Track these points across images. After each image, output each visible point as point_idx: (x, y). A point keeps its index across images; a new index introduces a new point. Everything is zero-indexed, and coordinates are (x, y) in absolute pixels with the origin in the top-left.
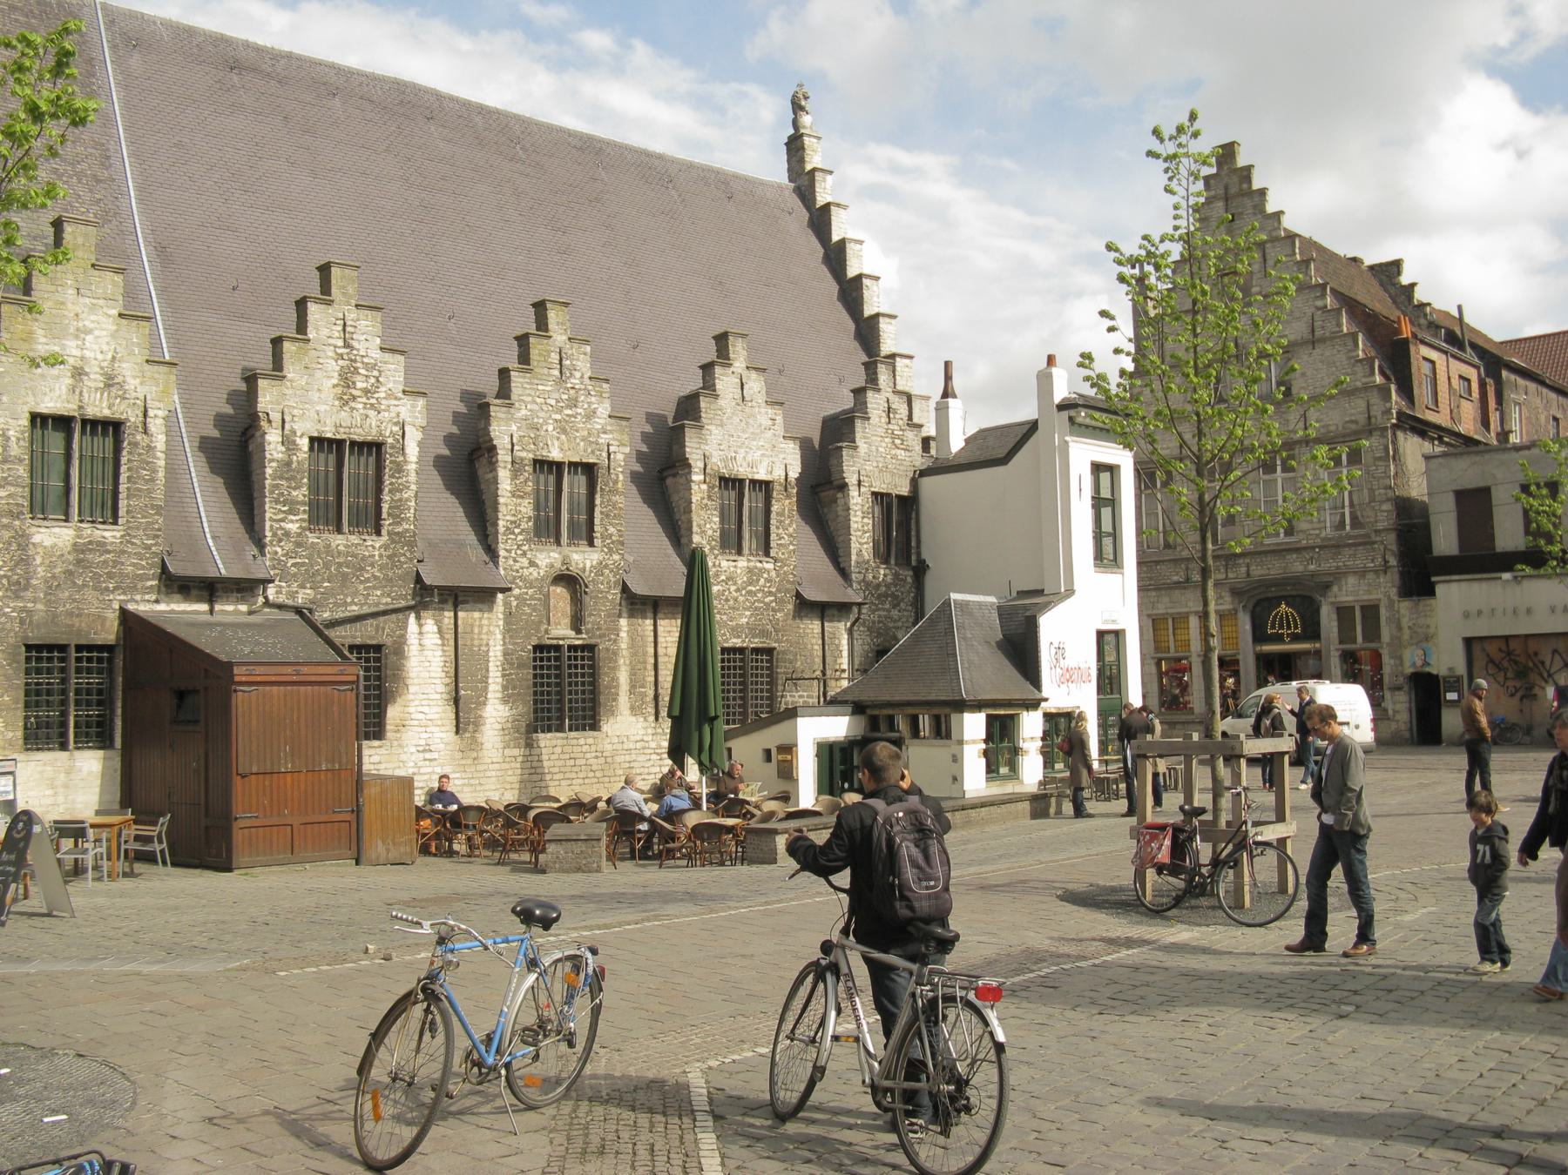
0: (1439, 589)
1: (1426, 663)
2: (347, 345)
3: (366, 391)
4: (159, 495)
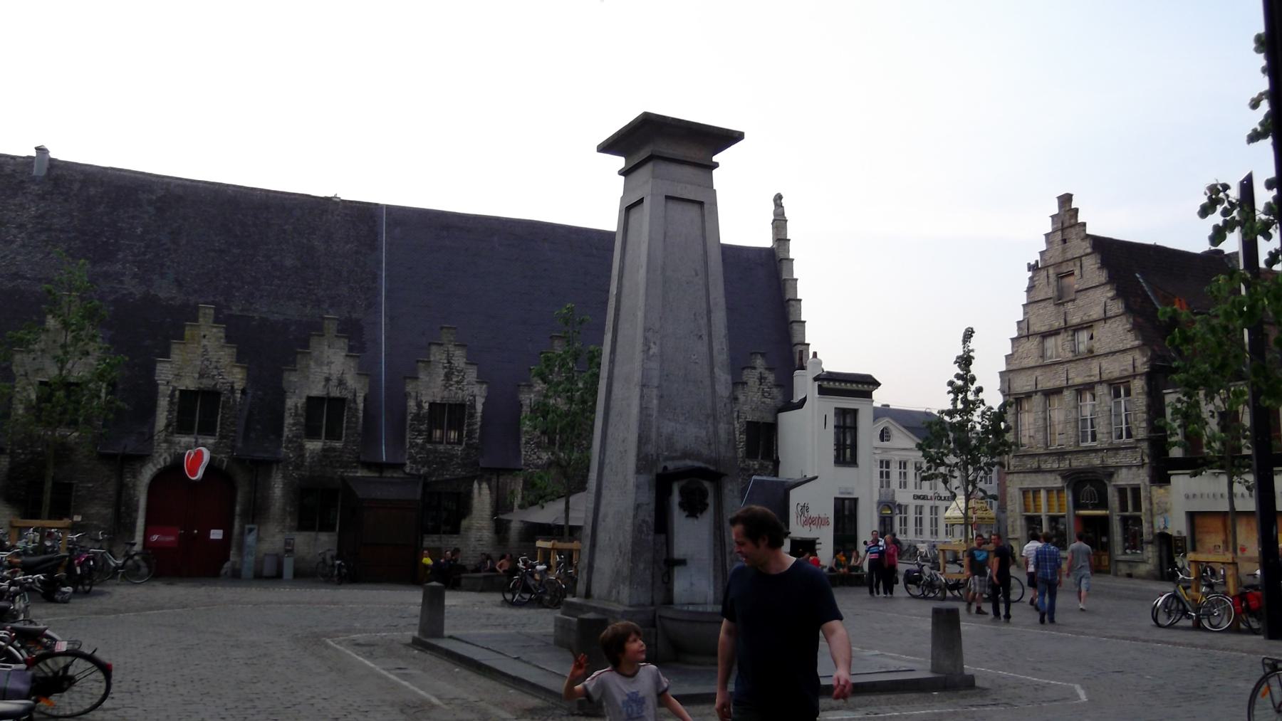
0: (1173, 479)
1: (1166, 528)
2: (449, 362)
3: (458, 382)
4: (360, 428)
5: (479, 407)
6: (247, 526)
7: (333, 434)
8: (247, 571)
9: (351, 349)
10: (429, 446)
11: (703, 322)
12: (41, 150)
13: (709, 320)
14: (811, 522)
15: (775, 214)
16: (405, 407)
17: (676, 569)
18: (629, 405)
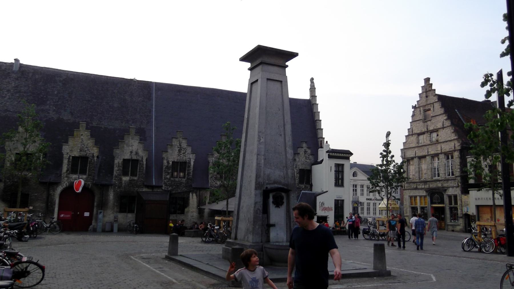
0: (470, 192)
1: (467, 211)
2: (180, 145)
3: (183, 153)
4: (144, 172)
5: (192, 163)
6: (99, 211)
7: (133, 174)
8: (99, 229)
9: (141, 140)
10: (172, 179)
11: (282, 129)
12: (16, 60)
13: (284, 128)
14: (325, 209)
15: (311, 86)
16: (162, 163)
17: (271, 228)
18: (252, 163)
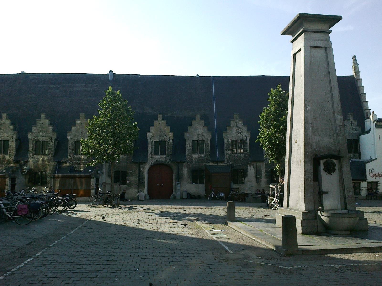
3: (240, 133)
4: (209, 150)
5: (248, 141)
6: (177, 183)
7: (201, 152)
8: (178, 197)
9: (205, 124)
10: (232, 155)
11: (329, 96)
12: (111, 71)
13: (332, 94)
14: (375, 175)
15: (354, 63)
16: (224, 142)
17: (324, 196)
18: (300, 131)
